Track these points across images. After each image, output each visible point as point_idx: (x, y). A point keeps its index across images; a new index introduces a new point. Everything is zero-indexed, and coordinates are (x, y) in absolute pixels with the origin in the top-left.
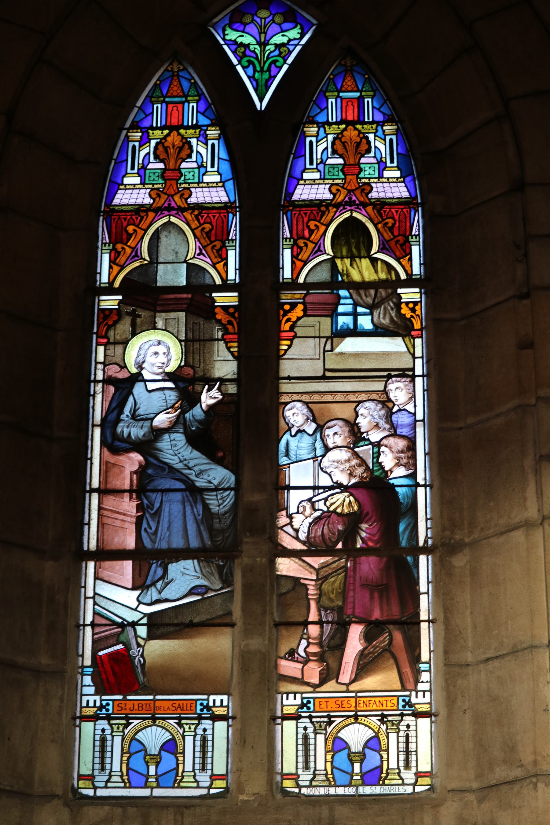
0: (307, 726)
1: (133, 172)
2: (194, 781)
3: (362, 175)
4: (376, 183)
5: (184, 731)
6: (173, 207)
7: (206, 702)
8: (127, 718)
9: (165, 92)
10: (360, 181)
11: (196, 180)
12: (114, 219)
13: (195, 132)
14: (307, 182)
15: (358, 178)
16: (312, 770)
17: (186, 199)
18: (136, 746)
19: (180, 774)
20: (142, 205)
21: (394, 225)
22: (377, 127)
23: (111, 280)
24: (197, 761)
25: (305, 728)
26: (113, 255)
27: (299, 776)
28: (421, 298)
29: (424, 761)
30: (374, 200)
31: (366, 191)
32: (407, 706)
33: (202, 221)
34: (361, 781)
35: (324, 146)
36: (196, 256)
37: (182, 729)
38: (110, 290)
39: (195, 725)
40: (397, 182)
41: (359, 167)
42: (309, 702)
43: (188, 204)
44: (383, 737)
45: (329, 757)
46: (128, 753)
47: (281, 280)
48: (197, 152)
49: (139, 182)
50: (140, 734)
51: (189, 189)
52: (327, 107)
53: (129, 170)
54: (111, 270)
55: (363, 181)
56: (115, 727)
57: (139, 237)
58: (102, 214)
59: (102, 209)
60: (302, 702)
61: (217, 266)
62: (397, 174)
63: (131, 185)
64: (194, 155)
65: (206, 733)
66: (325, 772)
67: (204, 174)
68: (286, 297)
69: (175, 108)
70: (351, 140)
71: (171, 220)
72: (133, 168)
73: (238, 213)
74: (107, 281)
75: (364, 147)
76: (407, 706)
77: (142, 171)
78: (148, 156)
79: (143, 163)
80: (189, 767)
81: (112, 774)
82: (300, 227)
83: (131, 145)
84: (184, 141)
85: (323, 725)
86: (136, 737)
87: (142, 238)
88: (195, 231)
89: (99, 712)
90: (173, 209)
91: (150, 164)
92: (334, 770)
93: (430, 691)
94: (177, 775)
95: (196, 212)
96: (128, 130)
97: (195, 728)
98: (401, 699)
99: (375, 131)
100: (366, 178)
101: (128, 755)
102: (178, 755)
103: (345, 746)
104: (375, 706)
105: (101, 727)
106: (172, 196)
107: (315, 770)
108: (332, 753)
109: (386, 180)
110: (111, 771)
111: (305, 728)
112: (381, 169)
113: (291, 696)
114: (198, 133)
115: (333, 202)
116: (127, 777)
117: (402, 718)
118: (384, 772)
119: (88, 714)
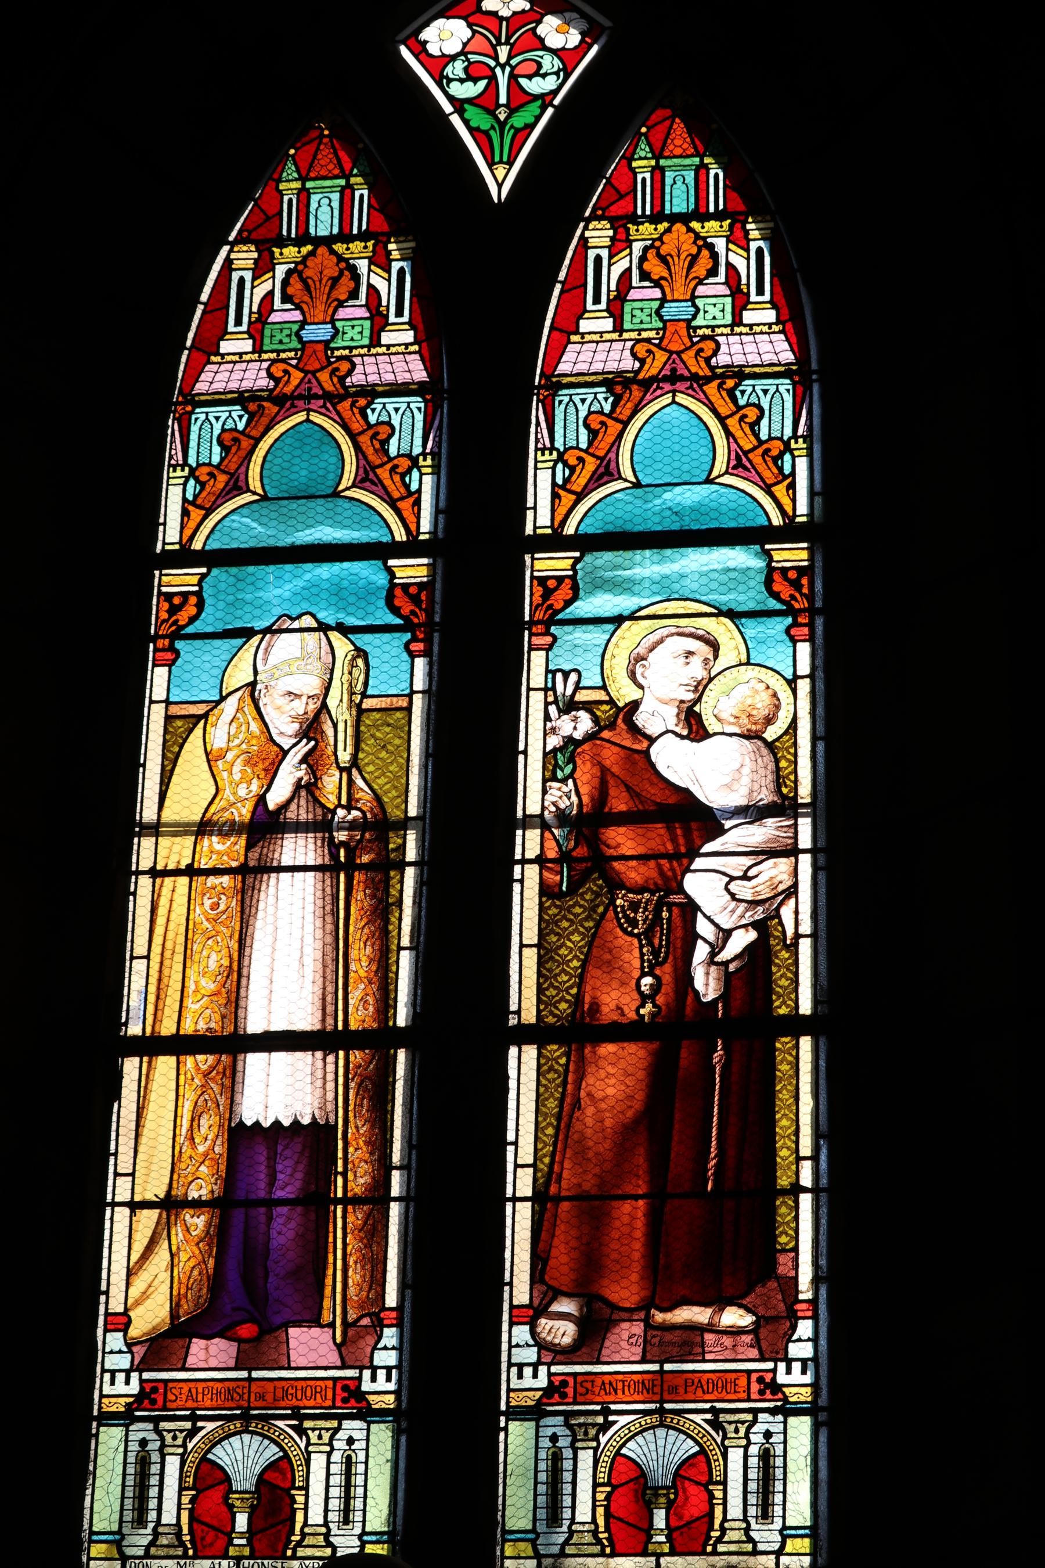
0: (772, 1430)
1: (760, 299)
4: (362, 356)
5: (308, 1444)
8: (194, 1418)
12: (560, 402)
13: (366, 247)
15: (689, 327)
17: (708, 360)
20: (620, 373)
22: (731, 226)
24: (334, 1504)
28: (811, 559)
33: (742, 402)
43: (712, 369)
47: (529, 530)
48: (729, 265)
49: (250, 349)
50: (218, 1450)
51: (347, 358)
58: (814, 377)
61: (774, 489)
63: (234, 354)
64: (722, 270)
66: (593, 1527)
69: (679, 180)
72: (238, 322)
73: (816, 388)
74: (177, 539)
79: (617, 290)
80: (735, 1510)
83: (592, 254)
84: (343, 265)
85: (181, 1436)
87: (620, 436)
90: (682, 378)
96: (233, 244)
97: (332, 1438)
98: (754, 1377)
100: (707, 327)
101: (608, 1489)
103: (221, 1475)
105: (141, 1435)
106: (314, 373)
112: (376, 329)
115: (641, 376)
117: (340, 1424)
118: (717, 1526)
119: (113, 1409)
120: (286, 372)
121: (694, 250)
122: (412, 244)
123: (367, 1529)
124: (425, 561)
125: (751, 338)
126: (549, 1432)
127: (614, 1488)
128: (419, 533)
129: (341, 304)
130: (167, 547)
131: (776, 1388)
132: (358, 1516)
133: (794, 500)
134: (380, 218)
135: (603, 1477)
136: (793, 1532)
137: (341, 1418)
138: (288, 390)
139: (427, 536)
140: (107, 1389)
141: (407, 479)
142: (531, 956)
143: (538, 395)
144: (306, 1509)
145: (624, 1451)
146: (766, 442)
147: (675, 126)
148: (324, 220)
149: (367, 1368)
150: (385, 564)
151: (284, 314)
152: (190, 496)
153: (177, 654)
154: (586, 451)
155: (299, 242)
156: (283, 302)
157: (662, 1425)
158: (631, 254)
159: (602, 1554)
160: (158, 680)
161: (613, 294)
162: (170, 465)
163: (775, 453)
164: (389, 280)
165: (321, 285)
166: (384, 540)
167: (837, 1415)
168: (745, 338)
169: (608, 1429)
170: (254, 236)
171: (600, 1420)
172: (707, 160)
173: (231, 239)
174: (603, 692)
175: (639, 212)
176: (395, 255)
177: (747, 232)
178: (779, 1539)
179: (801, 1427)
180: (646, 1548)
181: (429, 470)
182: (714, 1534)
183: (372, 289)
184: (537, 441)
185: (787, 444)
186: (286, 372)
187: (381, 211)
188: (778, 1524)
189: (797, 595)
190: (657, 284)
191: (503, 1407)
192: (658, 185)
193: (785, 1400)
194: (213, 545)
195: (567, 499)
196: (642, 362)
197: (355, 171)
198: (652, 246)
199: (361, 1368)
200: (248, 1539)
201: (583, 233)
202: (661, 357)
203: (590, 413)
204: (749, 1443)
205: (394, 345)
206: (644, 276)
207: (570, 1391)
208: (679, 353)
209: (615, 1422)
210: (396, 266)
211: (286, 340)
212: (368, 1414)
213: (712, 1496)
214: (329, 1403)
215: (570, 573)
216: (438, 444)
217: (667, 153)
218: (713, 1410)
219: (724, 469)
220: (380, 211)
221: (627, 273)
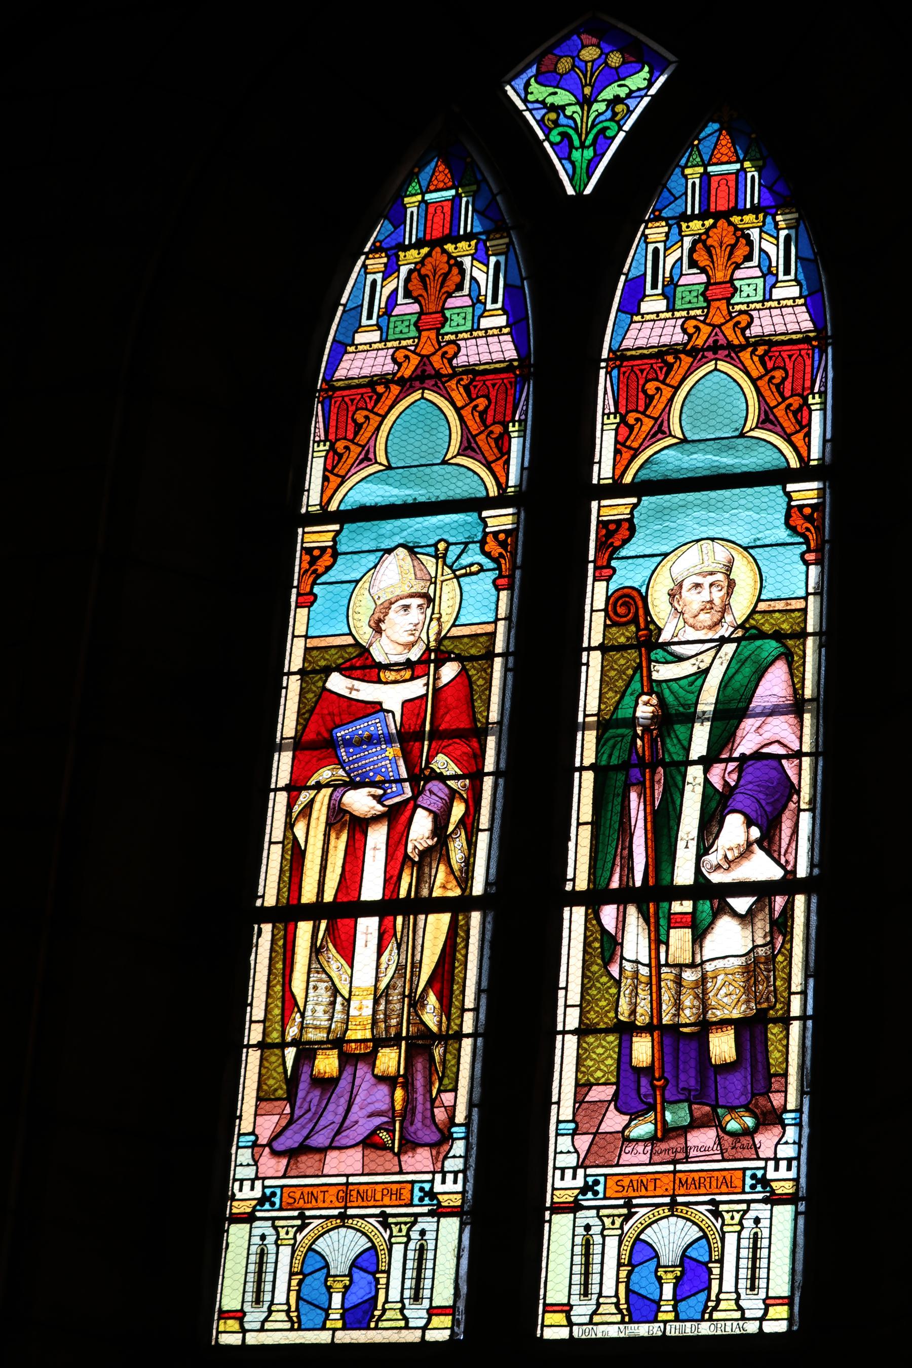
2: (616, 1312)
4: (759, 310)
5: (391, 1236)
6: (722, 345)
7: (762, 1172)
9: (424, 184)
10: (443, 338)
11: (468, 326)
12: (335, 402)
14: (647, 317)
15: (729, 304)
16: (266, 1305)
17: (450, 361)
18: (314, 1263)
19: (713, 1297)
21: (487, 407)
24: (743, 1273)
25: (263, 1237)
26: (329, 461)
27: (244, 1314)
31: (448, 356)
32: (426, 1199)
34: (341, 1322)
35: (677, 254)
37: (388, 1231)
41: (733, 285)
42: (596, 1183)
46: (300, 1274)
47: (595, 481)
52: (686, 193)
53: (364, 322)
54: (326, 483)
56: (282, 1232)
57: (664, 400)
58: (830, 341)
62: (795, 291)
67: (481, 316)
72: (654, 286)
73: (830, 350)
77: (670, 292)
78: (679, 263)
80: (394, 1295)
81: (274, 1308)
84: (739, 233)
85: (292, 1231)
87: (671, 400)
88: (462, 412)
89: (580, 1197)
90: (722, 347)
92: (301, 1303)
93: (464, 1171)
94: (708, 1299)
95: (761, 350)
98: (417, 1187)
100: (452, 334)
101: (301, 1277)
102: (378, 1276)
109: (775, 304)
110: (272, 1303)
111: (263, 1237)
115: (689, 347)
116: (295, 1314)
117: (749, 1207)
118: (380, 1307)
120: (407, 357)
122: (796, 215)
123: (770, 1295)
124: (510, 510)
125: (778, 311)
126: (584, 1222)
128: (809, 460)
129: (450, 295)
131: (765, 1182)
132: (763, 1283)
134: (767, 195)
135: (625, 1259)
138: (700, 342)
139: (815, 463)
141: (500, 442)
142: (586, 833)
143: (318, 398)
144: (721, 1279)
145: (642, 1237)
153: (614, 570)
155: (702, 217)
156: (690, 267)
157: (343, 1226)
158: (682, 246)
159: (622, 1322)
160: (299, 620)
162: (314, 442)
164: (777, 245)
165: (719, 254)
166: (479, 495)
167: (822, 1204)
169: (631, 1218)
172: (747, 164)
173: (366, 250)
174: (350, 637)
176: (782, 225)
177: (776, 224)
178: (763, 1307)
182: (711, 1304)
185: (806, 399)
186: (407, 357)
190: (703, 270)
191: (548, 1204)
193: (773, 1191)
194: (645, 475)
195: (627, 455)
199: (434, 1173)
201: (644, 231)
204: (743, 1228)
207: (277, 1200)
208: (719, 326)
211: (406, 330)
212: (774, 1200)
213: (377, 1281)
218: (712, 1202)
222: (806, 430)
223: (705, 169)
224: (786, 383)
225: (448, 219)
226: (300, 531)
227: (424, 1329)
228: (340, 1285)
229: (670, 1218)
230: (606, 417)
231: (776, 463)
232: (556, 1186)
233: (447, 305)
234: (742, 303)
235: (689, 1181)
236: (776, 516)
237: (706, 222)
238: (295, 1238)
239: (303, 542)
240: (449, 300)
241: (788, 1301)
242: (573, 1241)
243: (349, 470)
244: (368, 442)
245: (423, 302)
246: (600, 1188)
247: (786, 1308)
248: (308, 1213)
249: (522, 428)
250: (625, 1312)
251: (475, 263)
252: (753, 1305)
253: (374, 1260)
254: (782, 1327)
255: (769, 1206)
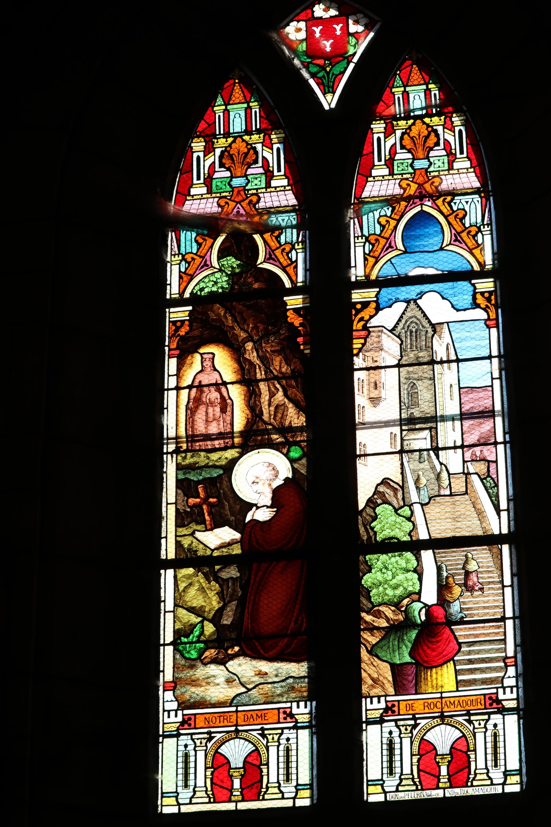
2: (412, 783)
3: (431, 169)
4: (445, 175)
5: (474, 728)
6: (242, 214)
8: (414, 718)
10: (430, 174)
16: (398, 776)
17: (254, 205)
23: (181, 292)
28: (495, 286)
29: (513, 758)
30: (261, 211)
32: (495, 704)
33: (455, 208)
36: (395, 248)
38: (180, 302)
39: (278, 735)
40: (284, 191)
42: (393, 706)
44: (263, 750)
45: (415, 759)
47: (168, 297)
49: (206, 192)
50: (223, 747)
51: (257, 194)
55: (250, 192)
57: (391, 227)
58: (491, 194)
59: (352, 202)
60: (387, 705)
63: (282, 187)
65: (187, 749)
68: (357, 296)
69: (417, 97)
70: (239, 152)
71: (424, 209)
73: (491, 198)
74: (363, 274)
75: (251, 157)
76: (495, 704)
79: (208, 173)
80: (481, 764)
81: (196, 789)
82: (371, 223)
84: (430, 129)
86: (219, 751)
87: (395, 227)
91: (216, 173)
94: (469, 773)
97: (279, 739)
99: (262, 141)
100: (254, 189)
101: (212, 770)
102: (469, 753)
104: (459, 707)
107: (402, 774)
108: (419, 757)
109: (456, 172)
110: (195, 786)
111: (186, 746)
113: (375, 700)
114: (443, 120)
116: (211, 793)
118: (472, 773)
121: (246, 150)
124: (301, 297)
127: (421, 756)
129: (431, 149)
130: (173, 296)
133: (296, 275)
135: (416, 751)
136: (509, 773)
137: (489, 714)
138: (412, 193)
139: (301, 284)
140: (369, 706)
141: (290, 255)
144: (268, 775)
145: (425, 738)
146: (469, 227)
147: (235, 88)
148: (238, 125)
149: (368, 697)
150: (470, 283)
151: (402, 155)
152: (367, 252)
154: (196, 254)
156: (220, 167)
161: (387, 158)
163: (473, 233)
168: (455, 176)
170: (202, 134)
171: (412, 722)
175: (217, 133)
178: (295, 790)
179: (512, 721)
180: (230, 798)
181: (301, 251)
182: (263, 790)
183: (264, 159)
184: (171, 249)
185: (479, 228)
186: (226, 203)
187: (266, 119)
188: (294, 783)
189: (489, 305)
191: (364, 719)
192: (226, 120)
193: (296, 722)
195: (371, 260)
196: (405, 190)
197: (431, 82)
198: (226, 150)
200: (241, 792)
202: (232, 204)
203: (380, 216)
204: (280, 744)
205: (279, 187)
206: (403, 147)
207: (282, 716)
209: (215, 737)
210: (275, 147)
212: (503, 711)
213: (469, 757)
214: (483, 707)
215: (375, 299)
216: (304, 236)
217: (410, 84)
219: (263, 260)
220: (266, 119)
221: (394, 146)
222: (295, 264)
223: (405, 89)
224: (466, 218)
225: (243, 119)
226: (167, 310)
227: (294, 798)
228: (446, 760)
229: (236, 740)
230: (356, 238)
231: (464, 266)
232: (368, 708)
233: (248, 173)
234: (436, 171)
235: (456, 703)
236: (466, 297)
237: (408, 121)
238: (206, 746)
239: (169, 318)
240: (431, 152)
241: (519, 772)
242: (382, 742)
243: (195, 272)
244: (206, 254)
245: (413, 152)
246: (396, 709)
247: (308, 791)
248: (417, 716)
249: (304, 246)
250: (418, 783)
251: (264, 148)
252: (497, 776)
253: (465, 743)
254: (517, 789)
255: (295, 731)
